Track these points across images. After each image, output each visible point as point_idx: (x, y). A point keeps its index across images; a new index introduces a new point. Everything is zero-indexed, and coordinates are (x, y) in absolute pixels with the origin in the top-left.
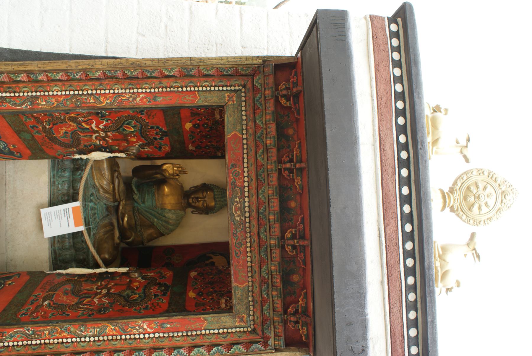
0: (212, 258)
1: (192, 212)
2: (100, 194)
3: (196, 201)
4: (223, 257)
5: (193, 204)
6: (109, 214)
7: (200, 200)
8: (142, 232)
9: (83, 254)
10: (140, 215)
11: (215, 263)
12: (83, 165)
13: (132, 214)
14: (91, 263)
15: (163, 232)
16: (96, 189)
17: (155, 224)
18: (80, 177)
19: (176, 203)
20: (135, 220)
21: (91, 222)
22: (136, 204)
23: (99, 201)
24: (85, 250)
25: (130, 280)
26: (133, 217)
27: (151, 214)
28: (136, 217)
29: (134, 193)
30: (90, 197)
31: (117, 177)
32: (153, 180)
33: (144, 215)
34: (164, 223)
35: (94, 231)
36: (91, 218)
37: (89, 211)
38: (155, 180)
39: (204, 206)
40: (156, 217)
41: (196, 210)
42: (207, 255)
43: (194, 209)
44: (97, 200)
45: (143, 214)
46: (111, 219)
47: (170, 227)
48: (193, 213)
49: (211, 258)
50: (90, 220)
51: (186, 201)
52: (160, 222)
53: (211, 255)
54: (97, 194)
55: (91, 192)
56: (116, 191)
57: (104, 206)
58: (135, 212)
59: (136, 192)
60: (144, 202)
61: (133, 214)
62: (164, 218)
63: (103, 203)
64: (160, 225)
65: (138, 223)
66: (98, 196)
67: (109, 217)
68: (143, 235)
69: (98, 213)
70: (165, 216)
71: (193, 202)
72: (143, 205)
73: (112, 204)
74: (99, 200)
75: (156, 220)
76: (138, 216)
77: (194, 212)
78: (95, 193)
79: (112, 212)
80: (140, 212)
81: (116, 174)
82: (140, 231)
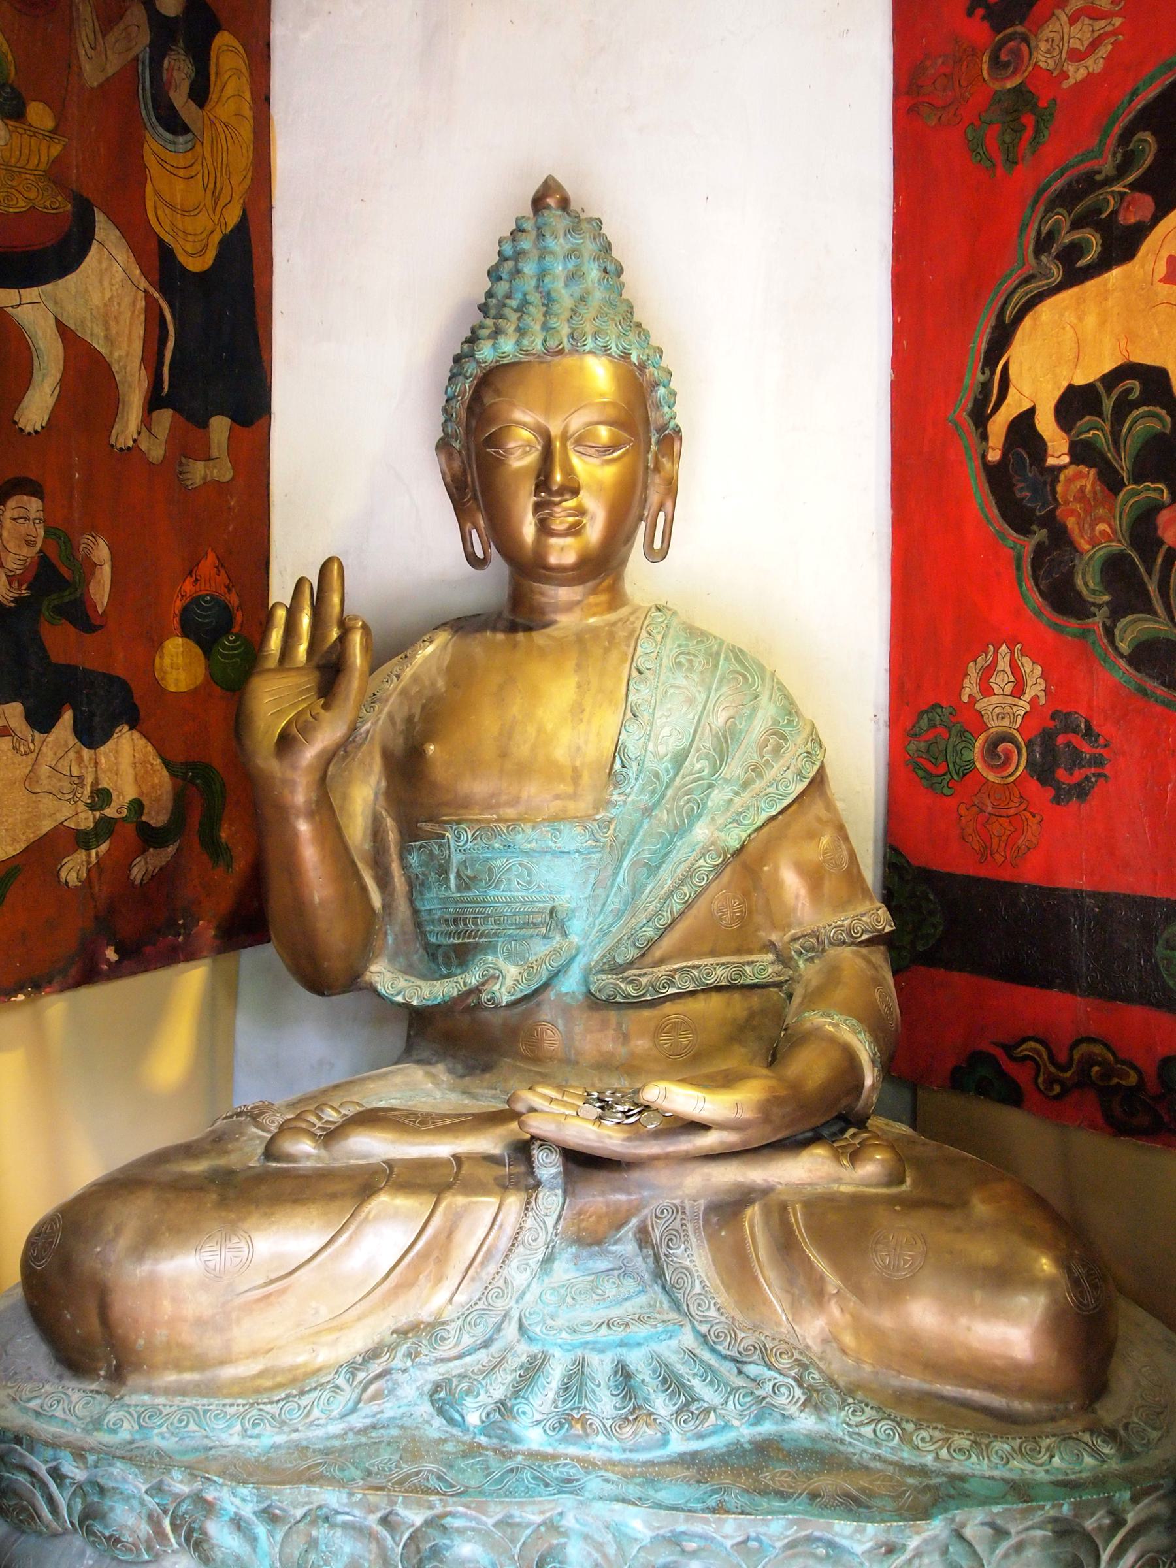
0: (1025, 422)
1: (657, 555)
2: (449, 1313)
3: (572, 503)
4: (1027, 322)
5: (594, 532)
6: (634, 1221)
7: (558, 477)
8: (795, 939)
9: (1004, 1546)
10: (657, 953)
11: (1071, 387)
12: (157, 1489)
13: (646, 1013)
14: (1089, 1460)
15: (800, 775)
16: (397, 1363)
17: (733, 839)
18: (261, 1530)
19: (579, 667)
20: (693, 993)
21: (701, 1436)
22: (570, 984)
23: (511, 1331)
24: (968, 1532)
25: (188, 629)
26: (668, 1008)
27: (653, 869)
28: (671, 983)
29: (476, 990)
30: (462, 1424)
31: (330, 1136)
32: (392, 836)
33: (666, 918)
34: (734, 769)
35: (782, 1400)
36: (665, 1443)
37: (595, 1454)
38: (389, 822)
39: (613, 447)
40: (680, 830)
41: (642, 526)
42: (994, 456)
43: (630, 538)
44: (495, 1348)
45: (650, 932)
46: (678, 1210)
47: (759, 726)
48: (664, 554)
49: (1025, 422)
50: (678, 1445)
51: (564, 594)
52: (717, 797)
53: (999, 425)
54: (445, 1350)
55: (426, 1408)
56: (442, 1148)
57: (563, 1269)
58: (630, 989)
59: (473, 978)
60: (555, 920)
61: (652, 1004)
62: (696, 764)
63: (535, 1289)
64: (746, 795)
65: (720, 975)
66: (467, 1341)
67: (656, 1234)
68: (815, 934)
69: (622, 1344)
70: (679, 759)
71: (575, 530)
72: (576, 926)
73: (550, 1201)
74: (498, 1328)
75: (701, 832)
76: (662, 971)
77: (657, 545)
78: (434, 1374)
79: (622, 1197)
80: (632, 953)
81: (304, 1148)
82: (783, 959)
